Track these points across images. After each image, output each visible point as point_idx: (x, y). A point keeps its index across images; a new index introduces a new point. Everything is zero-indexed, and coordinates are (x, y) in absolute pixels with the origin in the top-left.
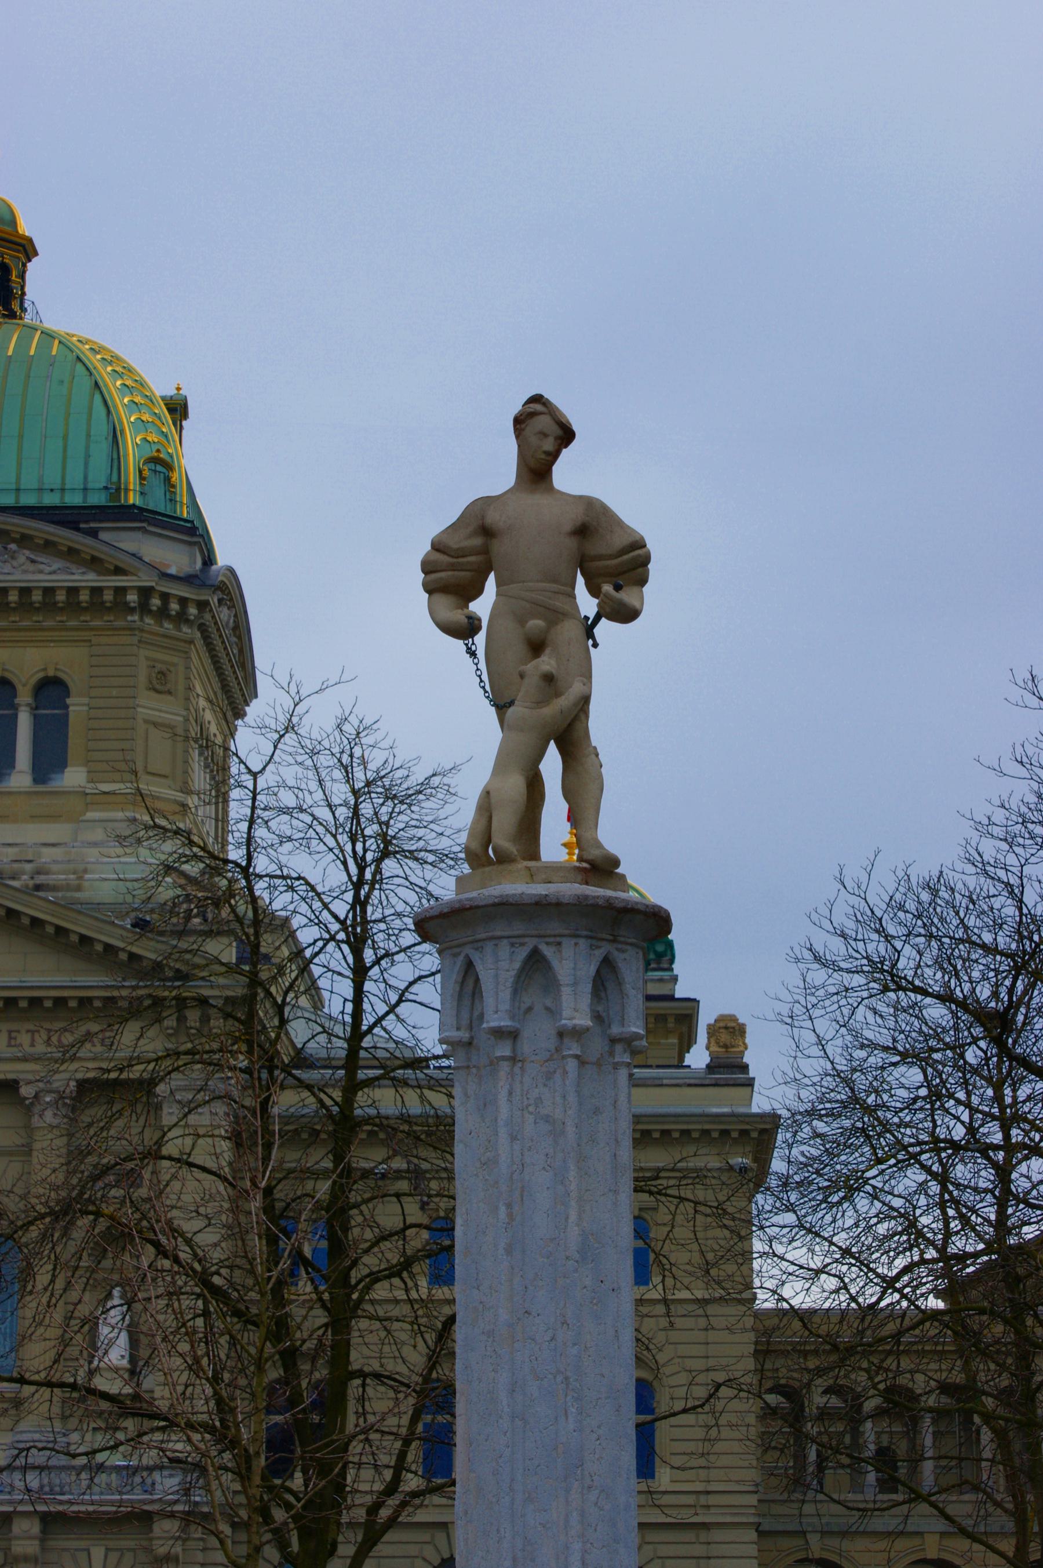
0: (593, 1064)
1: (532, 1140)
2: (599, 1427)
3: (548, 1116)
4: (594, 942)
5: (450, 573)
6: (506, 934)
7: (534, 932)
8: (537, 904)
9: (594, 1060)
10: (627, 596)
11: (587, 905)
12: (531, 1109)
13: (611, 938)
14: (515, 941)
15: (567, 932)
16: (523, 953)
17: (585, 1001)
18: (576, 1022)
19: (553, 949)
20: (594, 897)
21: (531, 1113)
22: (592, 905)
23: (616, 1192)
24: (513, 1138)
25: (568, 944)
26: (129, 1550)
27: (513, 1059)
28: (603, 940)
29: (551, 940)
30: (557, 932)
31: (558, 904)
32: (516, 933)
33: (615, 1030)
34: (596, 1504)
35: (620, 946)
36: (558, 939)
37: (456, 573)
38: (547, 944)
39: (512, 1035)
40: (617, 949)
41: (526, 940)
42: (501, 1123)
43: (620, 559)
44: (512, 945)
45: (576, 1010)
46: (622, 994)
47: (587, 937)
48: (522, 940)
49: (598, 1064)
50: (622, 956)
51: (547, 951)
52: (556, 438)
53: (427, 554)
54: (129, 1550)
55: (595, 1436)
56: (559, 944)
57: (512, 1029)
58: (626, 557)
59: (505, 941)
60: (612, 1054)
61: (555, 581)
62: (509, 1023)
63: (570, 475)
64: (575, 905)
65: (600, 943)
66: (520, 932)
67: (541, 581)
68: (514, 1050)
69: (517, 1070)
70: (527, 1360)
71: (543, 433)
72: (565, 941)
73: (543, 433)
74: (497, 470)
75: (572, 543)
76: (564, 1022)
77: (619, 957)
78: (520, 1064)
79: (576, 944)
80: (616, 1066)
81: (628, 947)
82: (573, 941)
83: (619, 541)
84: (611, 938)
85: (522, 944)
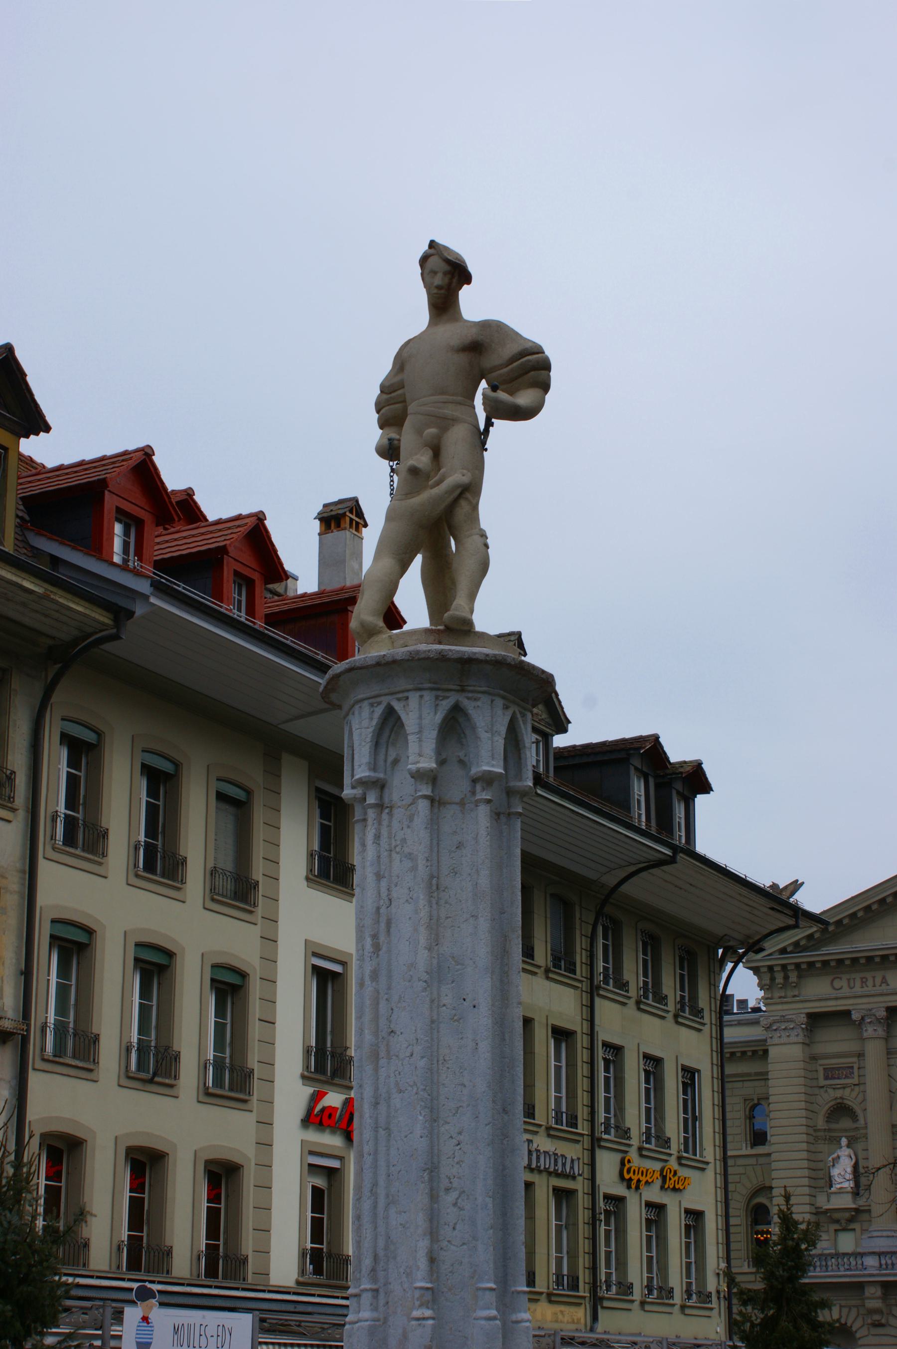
0: (457, 804)
1: (398, 877)
2: (460, 1133)
3: (410, 854)
4: (439, 693)
5: (387, 408)
6: (368, 695)
7: (387, 691)
8: (378, 664)
9: (457, 800)
10: (524, 399)
11: (419, 659)
12: (398, 849)
13: (459, 688)
14: (373, 700)
15: (411, 687)
16: (379, 711)
17: (430, 745)
18: (420, 765)
19: (402, 704)
20: (425, 651)
21: (398, 853)
22: (424, 659)
23: (475, 917)
24: (379, 876)
25: (414, 697)
26: (854, 1306)
27: (380, 806)
28: (451, 690)
29: (400, 695)
30: (403, 688)
31: (394, 662)
32: (373, 693)
33: (474, 771)
34: (455, 1204)
35: (470, 695)
36: (406, 694)
37: (392, 406)
38: (399, 700)
39: (380, 785)
40: (468, 698)
41: (382, 698)
42: (368, 864)
43: (510, 367)
44: (372, 705)
45: (420, 755)
46: (478, 738)
47: (432, 689)
48: (378, 699)
49: (462, 803)
50: (473, 704)
51: (397, 706)
52: (445, 274)
53: (379, 397)
54: (854, 1306)
55: (455, 1141)
56: (407, 698)
57: (374, 780)
58: (515, 364)
59: (366, 703)
60: (474, 793)
61: (443, 393)
62: (367, 774)
63: (473, 304)
64: (408, 660)
65: (447, 694)
66: (376, 693)
67: (432, 395)
68: (381, 797)
69: (385, 816)
70: (392, 1075)
71: (446, 275)
72: (410, 694)
73: (446, 275)
74: (413, 314)
75: (462, 359)
76: (410, 766)
77: (469, 705)
78: (387, 811)
79: (421, 697)
80: (477, 803)
81: (479, 695)
82: (418, 694)
83: (511, 350)
84: (459, 688)
85: (379, 703)
